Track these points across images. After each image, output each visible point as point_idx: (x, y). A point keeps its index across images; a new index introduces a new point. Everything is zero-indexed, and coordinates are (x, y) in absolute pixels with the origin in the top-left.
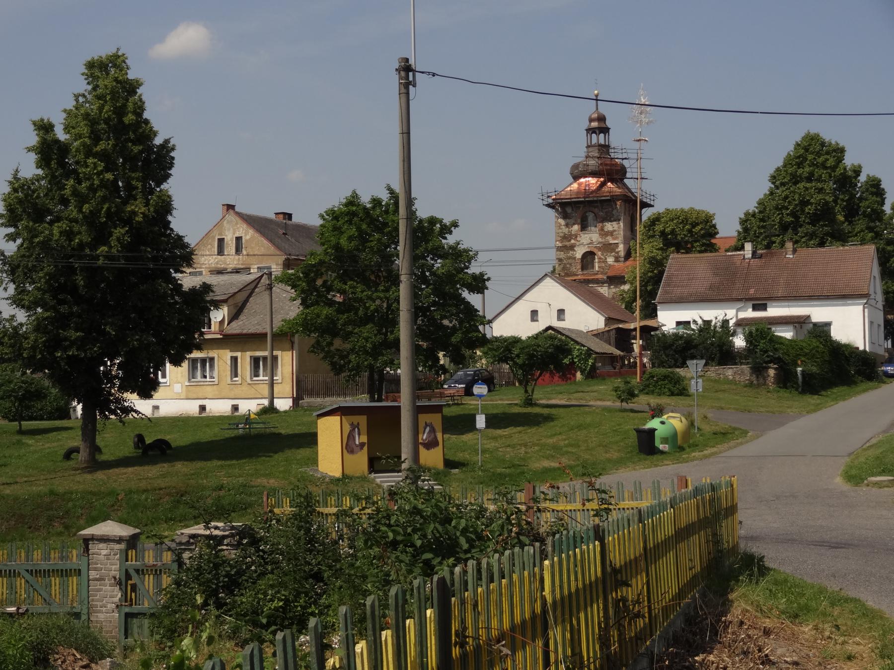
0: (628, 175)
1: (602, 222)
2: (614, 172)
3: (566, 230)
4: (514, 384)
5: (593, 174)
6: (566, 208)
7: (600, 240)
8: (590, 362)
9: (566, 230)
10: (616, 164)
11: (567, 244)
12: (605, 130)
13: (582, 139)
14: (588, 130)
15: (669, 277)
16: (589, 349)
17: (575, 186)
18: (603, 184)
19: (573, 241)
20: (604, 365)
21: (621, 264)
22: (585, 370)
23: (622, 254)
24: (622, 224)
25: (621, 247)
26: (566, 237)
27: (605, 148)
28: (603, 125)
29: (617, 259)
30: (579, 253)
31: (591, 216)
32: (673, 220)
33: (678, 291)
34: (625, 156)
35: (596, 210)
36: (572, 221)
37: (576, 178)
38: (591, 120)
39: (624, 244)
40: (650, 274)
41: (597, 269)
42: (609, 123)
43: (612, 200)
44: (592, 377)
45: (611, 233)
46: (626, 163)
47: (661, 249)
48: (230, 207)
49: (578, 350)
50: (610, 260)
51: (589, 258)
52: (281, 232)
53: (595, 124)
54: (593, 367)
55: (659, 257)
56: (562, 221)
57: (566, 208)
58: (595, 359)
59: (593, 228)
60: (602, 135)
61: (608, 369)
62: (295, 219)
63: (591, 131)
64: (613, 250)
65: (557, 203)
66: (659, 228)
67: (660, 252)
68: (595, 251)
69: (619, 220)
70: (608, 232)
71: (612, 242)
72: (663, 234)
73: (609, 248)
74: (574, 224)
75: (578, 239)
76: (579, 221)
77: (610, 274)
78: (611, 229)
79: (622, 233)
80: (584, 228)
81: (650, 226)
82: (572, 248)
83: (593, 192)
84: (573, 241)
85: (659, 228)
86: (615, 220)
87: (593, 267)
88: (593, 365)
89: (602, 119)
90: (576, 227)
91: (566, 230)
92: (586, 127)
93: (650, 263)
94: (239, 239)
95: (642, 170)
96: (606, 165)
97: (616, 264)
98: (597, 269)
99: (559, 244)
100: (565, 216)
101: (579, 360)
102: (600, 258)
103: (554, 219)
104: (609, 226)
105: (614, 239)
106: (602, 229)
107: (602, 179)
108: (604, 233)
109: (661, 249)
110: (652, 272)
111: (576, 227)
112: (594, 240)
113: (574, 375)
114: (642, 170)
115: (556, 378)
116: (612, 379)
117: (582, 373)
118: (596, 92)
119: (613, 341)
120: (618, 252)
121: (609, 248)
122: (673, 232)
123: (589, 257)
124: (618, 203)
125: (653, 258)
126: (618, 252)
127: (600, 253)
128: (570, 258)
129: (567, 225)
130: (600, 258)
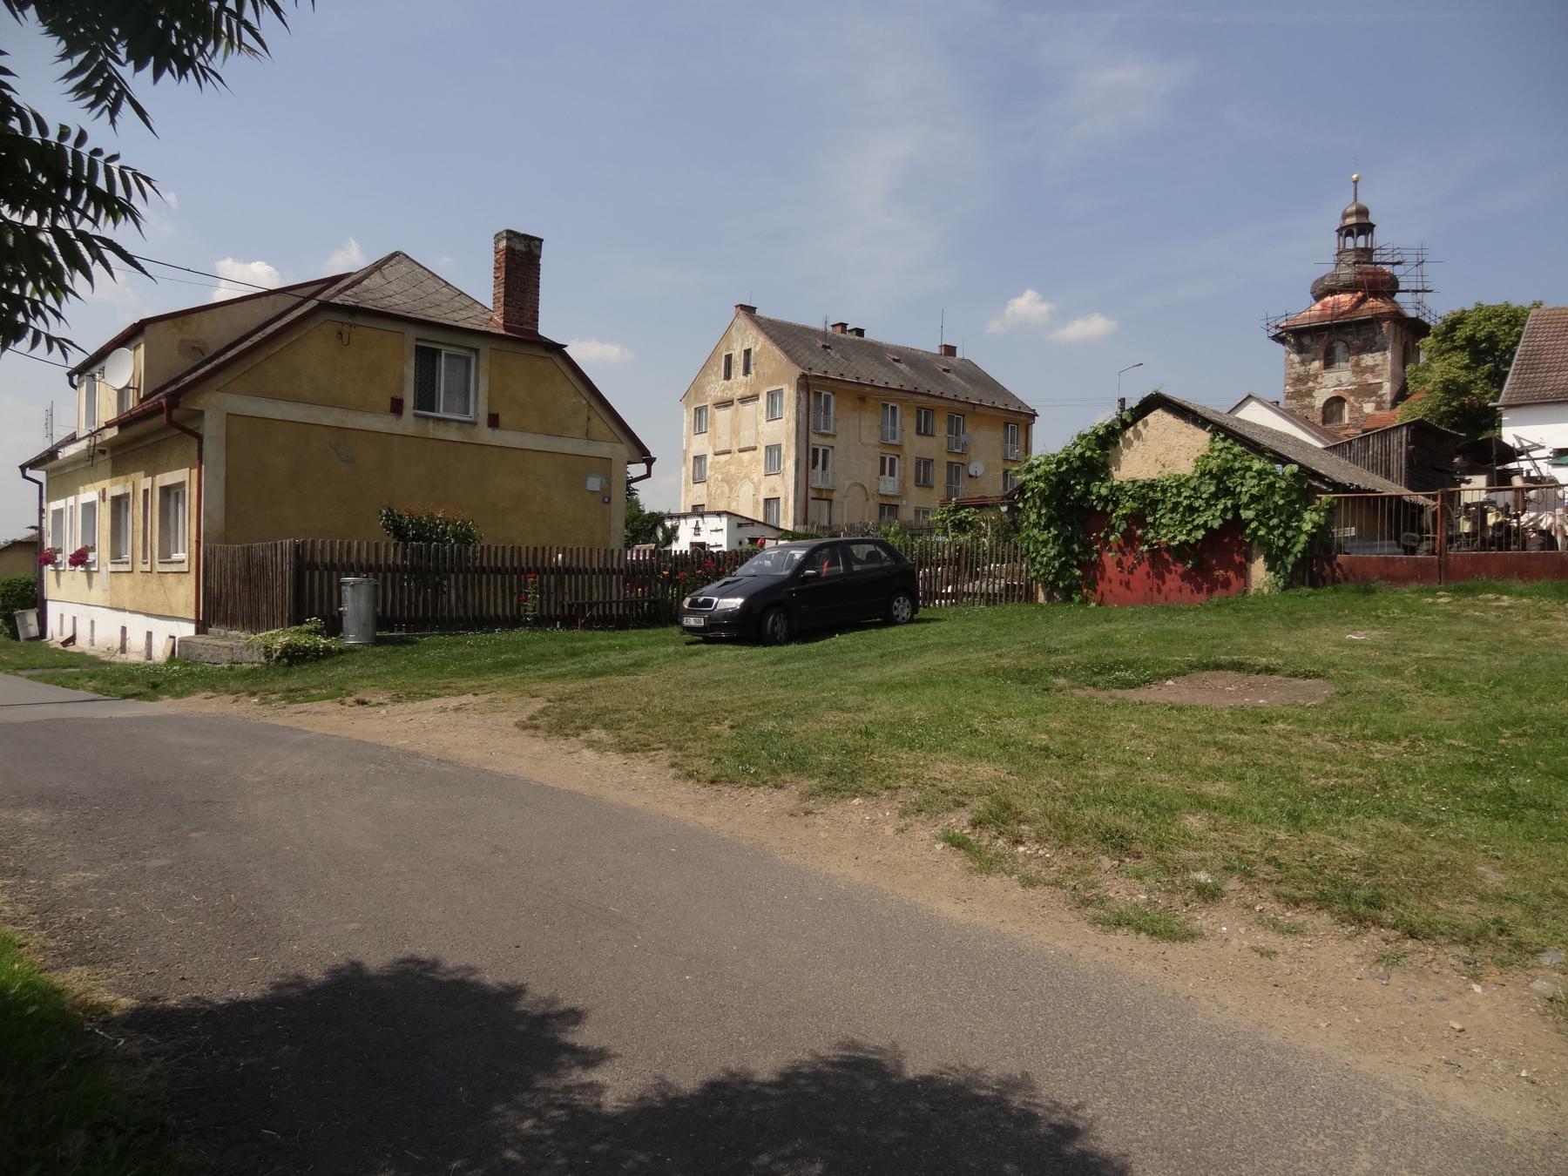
0: (1402, 287)
2: (1385, 287)
4: (1030, 596)
6: (1298, 337)
8: (1310, 520)
10: (1384, 273)
11: (1303, 388)
12: (1366, 228)
13: (1331, 243)
16: (1306, 473)
20: (1366, 535)
22: (1285, 551)
23: (1388, 398)
24: (1389, 355)
26: (1301, 379)
29: (1379, 407)
30: (1320, 399)
31: (1340, 347)
36: (1310, 356)
37: (1318, 298)
40: (1443, 409)
42: (1372, 219)
43: (1374, 322)
44: (1316, 582)
45: (1371, 369)
46: (1397, 271)
47: (1467, 367)
48: (749, 310)
49: (1261, 474)
50: (1369, 408)
51: (1335, 407)
52: (820, 344)
53: (1351, 220)
54: (1322, 543)
55: (1462, 380)
56: (1295, 358)
57: (1298, 337)
58: (1331, 510)
59: (1343, 364)
60: (1362, 238)
61: (1385, 550)
62: (868, 336)
63: (1346, 231)
64: (1374, 393)
66: (1462, 333)
67: (1464, 372)
68: (1345, 395)
72: (1471, 341)
73: (1367, 391)
80: (1328, 364)
81: (1447, 333)
82: (1309, 393)
84: (1311, 384)
85: (1462, 333)
87: (1341, 418)
88: (1322, 531)
89: (1362, 212)
90: (1317, 364)
91: (1301, 369)
93: (1446, 389)
94: (748, 352)
98: (1347, 421)
99: (1290, 389)
100: (1300, 349)
101: (1262, 516)
102: (1352, 406)
104: (1368, 359)
105: (1377, 377)
106: (1357, 364)
108: (1359, 370)
110: (1448, 404)
113: (1243, 572)
115: (1173, 581)
116: (1408, 593)
117: (1273, 563)
119: (1398, 461)
124: (1385, 325)
125: (1453, 381)
127: (1352, 399)
129: (1303, 362)
130: (1352, 406)
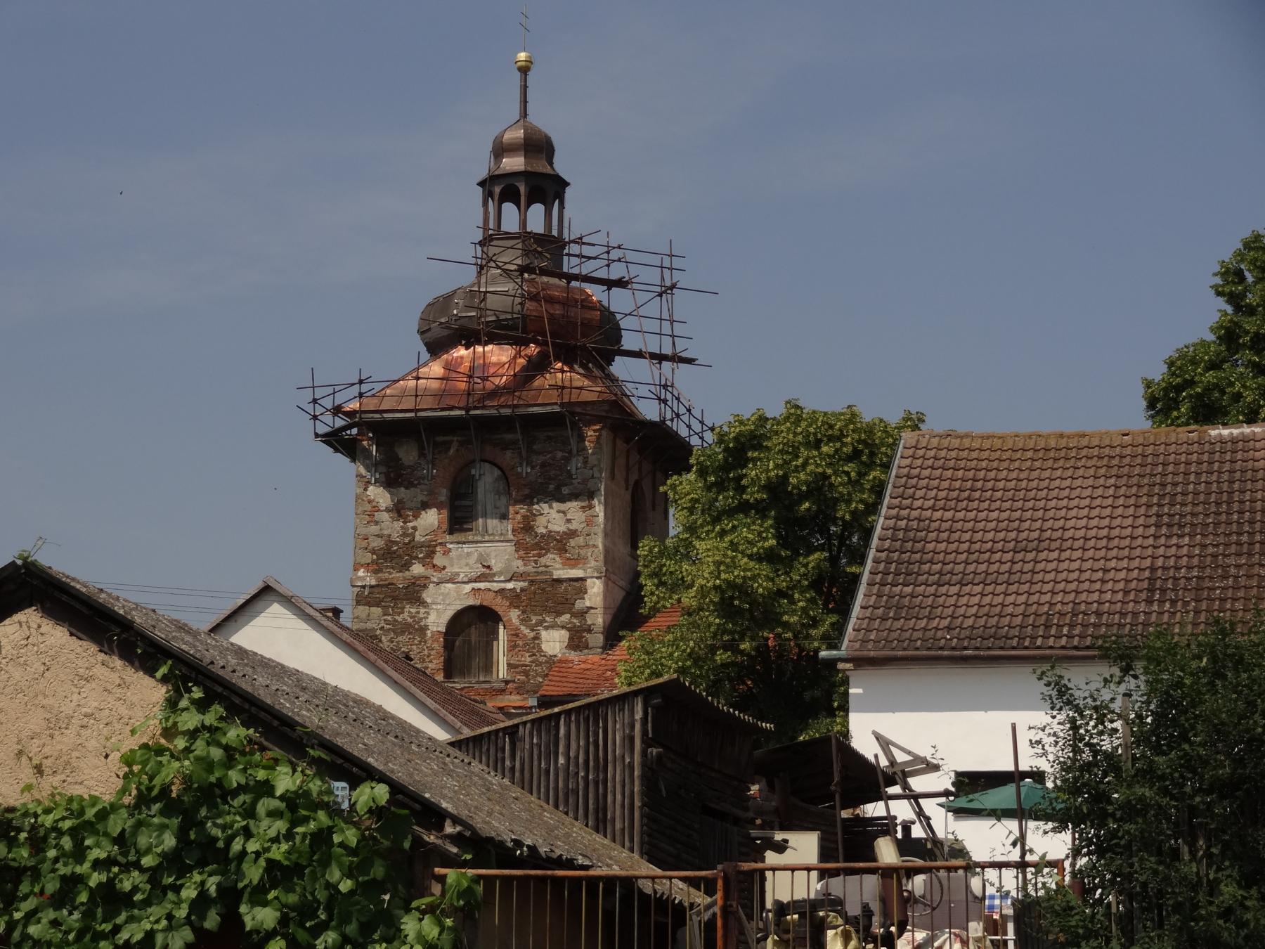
1: (529, 499)
2: (584, 336)
3: (393, 528)
5: (499, 332)
7: (518, 565)
9: (393, 528)
11: (397, 577)
12: (547, 188)
13: (466, 213)
14: (486, 184)
15: (902, 538)
17: (436, 369)
18: (538, 366)
19: (417, 569)
21: (594, 657)
23: (598, 620)
24: (599, 509)
25: (595, 592)
27: (546, 250)
28: (541, 167)
29: (577, 641)
31: (486, 479)
32: (817, 444)
33: (969, 605)
34: (616, 272)
35: (508, 457)
36: (419, 495)
37: (436, 348)
38: (500, 150)
39: (608, 578)
40: (721, 657)
41: (502, 672)
42: (562, 166)
43: (563, 422)
45: (560, 543)
46: (619, 301)
47: (769, 557)
49: (295, 805)
50: (554, 642)
51: (474, 634)
53: (514, 163)
55: (761, 587)
56: (380, 496)
59: (493, 523)
60: (537, 210)
65: (365, 426)
67: (765, 569)
68: (499, 605)
69: (591, 495)
70: (549, 535)
71: (561, 573)
73: (550, 598)
74: (425, 506)
75: (439, 560)
76: (444, 494)
77: (551, 690)
78: (558, 526)
79: (599, 541)
80: (459, 522)
81: (725, 467)
82: (413, 593)
83: (495, 393)
84: (417, 569)
86: (574, 496)
87: (488, 666)
90: (431, 519)
92: (483, 174)
93: (726, 608)
95: (678, 329)
96: (550, 300)
97: (573, 656)
98: (502, 672)
99: (366, 577)
103: (354, 488)
106: (527, 527)
107: (533, 349)
108: (531, 542)
109: (769, 557)
110: (731, 647)
111: (431, 519)
112: (497, 565)
114: (678, 329)
118: (522, 56)
119: (625, 789)
120: (583, 613)
121: (550, 598)
122: (819, 487)
123: (475, 623)
124: (590, 433)
125: (742, 589)
126: (583, 613)
128: (405, 628)
129: (398, 510)
130: (516, 634)
